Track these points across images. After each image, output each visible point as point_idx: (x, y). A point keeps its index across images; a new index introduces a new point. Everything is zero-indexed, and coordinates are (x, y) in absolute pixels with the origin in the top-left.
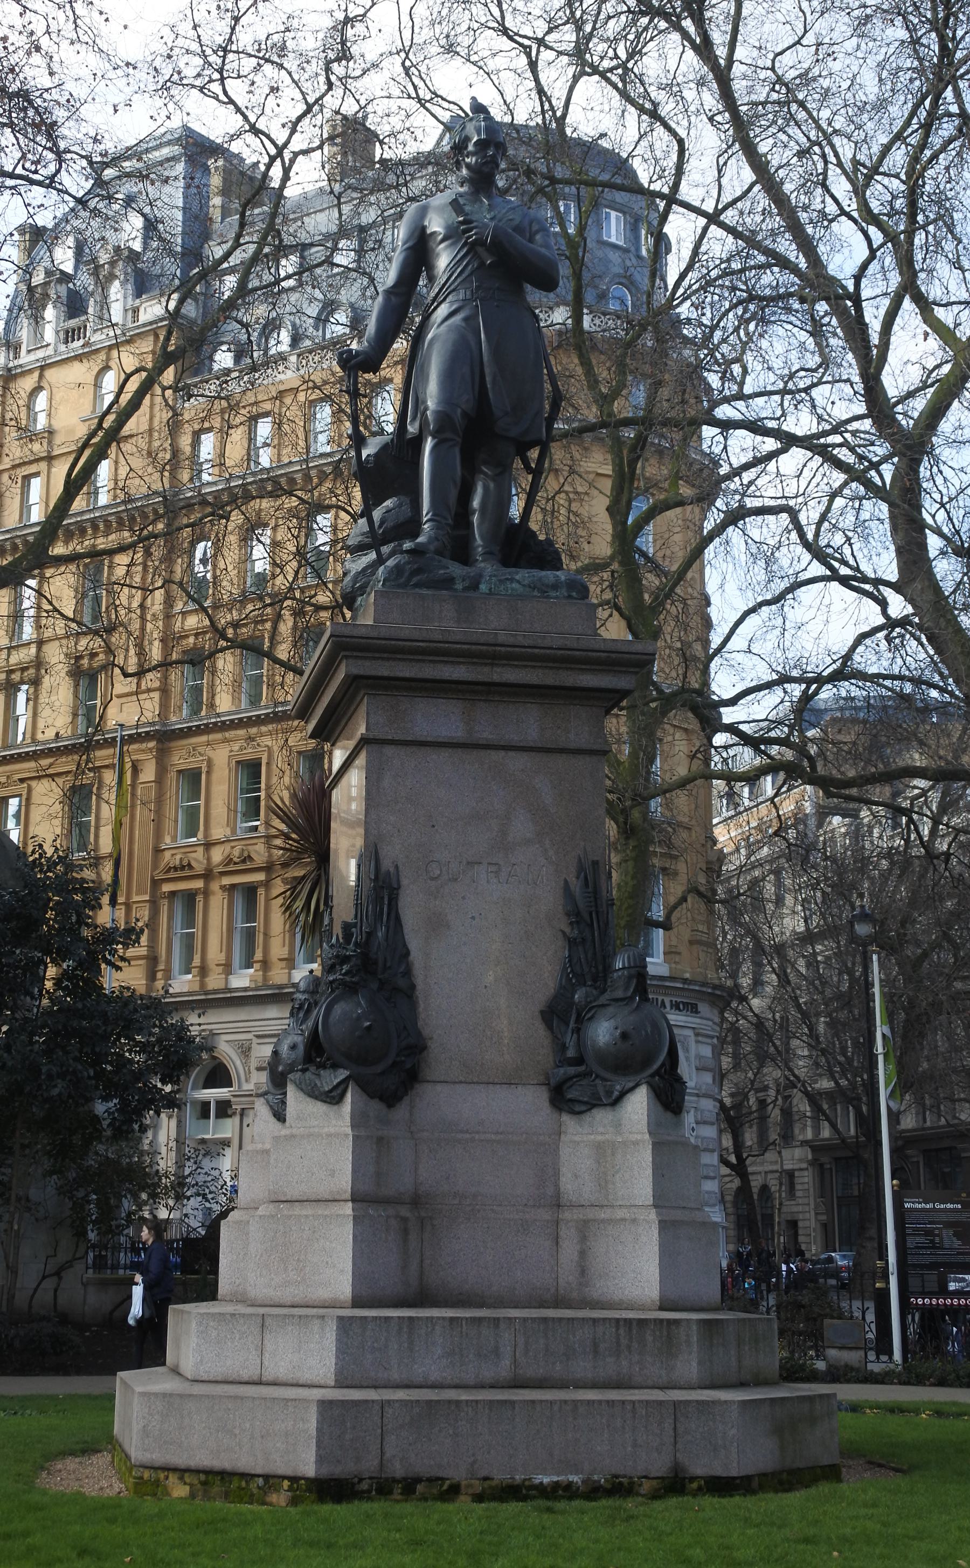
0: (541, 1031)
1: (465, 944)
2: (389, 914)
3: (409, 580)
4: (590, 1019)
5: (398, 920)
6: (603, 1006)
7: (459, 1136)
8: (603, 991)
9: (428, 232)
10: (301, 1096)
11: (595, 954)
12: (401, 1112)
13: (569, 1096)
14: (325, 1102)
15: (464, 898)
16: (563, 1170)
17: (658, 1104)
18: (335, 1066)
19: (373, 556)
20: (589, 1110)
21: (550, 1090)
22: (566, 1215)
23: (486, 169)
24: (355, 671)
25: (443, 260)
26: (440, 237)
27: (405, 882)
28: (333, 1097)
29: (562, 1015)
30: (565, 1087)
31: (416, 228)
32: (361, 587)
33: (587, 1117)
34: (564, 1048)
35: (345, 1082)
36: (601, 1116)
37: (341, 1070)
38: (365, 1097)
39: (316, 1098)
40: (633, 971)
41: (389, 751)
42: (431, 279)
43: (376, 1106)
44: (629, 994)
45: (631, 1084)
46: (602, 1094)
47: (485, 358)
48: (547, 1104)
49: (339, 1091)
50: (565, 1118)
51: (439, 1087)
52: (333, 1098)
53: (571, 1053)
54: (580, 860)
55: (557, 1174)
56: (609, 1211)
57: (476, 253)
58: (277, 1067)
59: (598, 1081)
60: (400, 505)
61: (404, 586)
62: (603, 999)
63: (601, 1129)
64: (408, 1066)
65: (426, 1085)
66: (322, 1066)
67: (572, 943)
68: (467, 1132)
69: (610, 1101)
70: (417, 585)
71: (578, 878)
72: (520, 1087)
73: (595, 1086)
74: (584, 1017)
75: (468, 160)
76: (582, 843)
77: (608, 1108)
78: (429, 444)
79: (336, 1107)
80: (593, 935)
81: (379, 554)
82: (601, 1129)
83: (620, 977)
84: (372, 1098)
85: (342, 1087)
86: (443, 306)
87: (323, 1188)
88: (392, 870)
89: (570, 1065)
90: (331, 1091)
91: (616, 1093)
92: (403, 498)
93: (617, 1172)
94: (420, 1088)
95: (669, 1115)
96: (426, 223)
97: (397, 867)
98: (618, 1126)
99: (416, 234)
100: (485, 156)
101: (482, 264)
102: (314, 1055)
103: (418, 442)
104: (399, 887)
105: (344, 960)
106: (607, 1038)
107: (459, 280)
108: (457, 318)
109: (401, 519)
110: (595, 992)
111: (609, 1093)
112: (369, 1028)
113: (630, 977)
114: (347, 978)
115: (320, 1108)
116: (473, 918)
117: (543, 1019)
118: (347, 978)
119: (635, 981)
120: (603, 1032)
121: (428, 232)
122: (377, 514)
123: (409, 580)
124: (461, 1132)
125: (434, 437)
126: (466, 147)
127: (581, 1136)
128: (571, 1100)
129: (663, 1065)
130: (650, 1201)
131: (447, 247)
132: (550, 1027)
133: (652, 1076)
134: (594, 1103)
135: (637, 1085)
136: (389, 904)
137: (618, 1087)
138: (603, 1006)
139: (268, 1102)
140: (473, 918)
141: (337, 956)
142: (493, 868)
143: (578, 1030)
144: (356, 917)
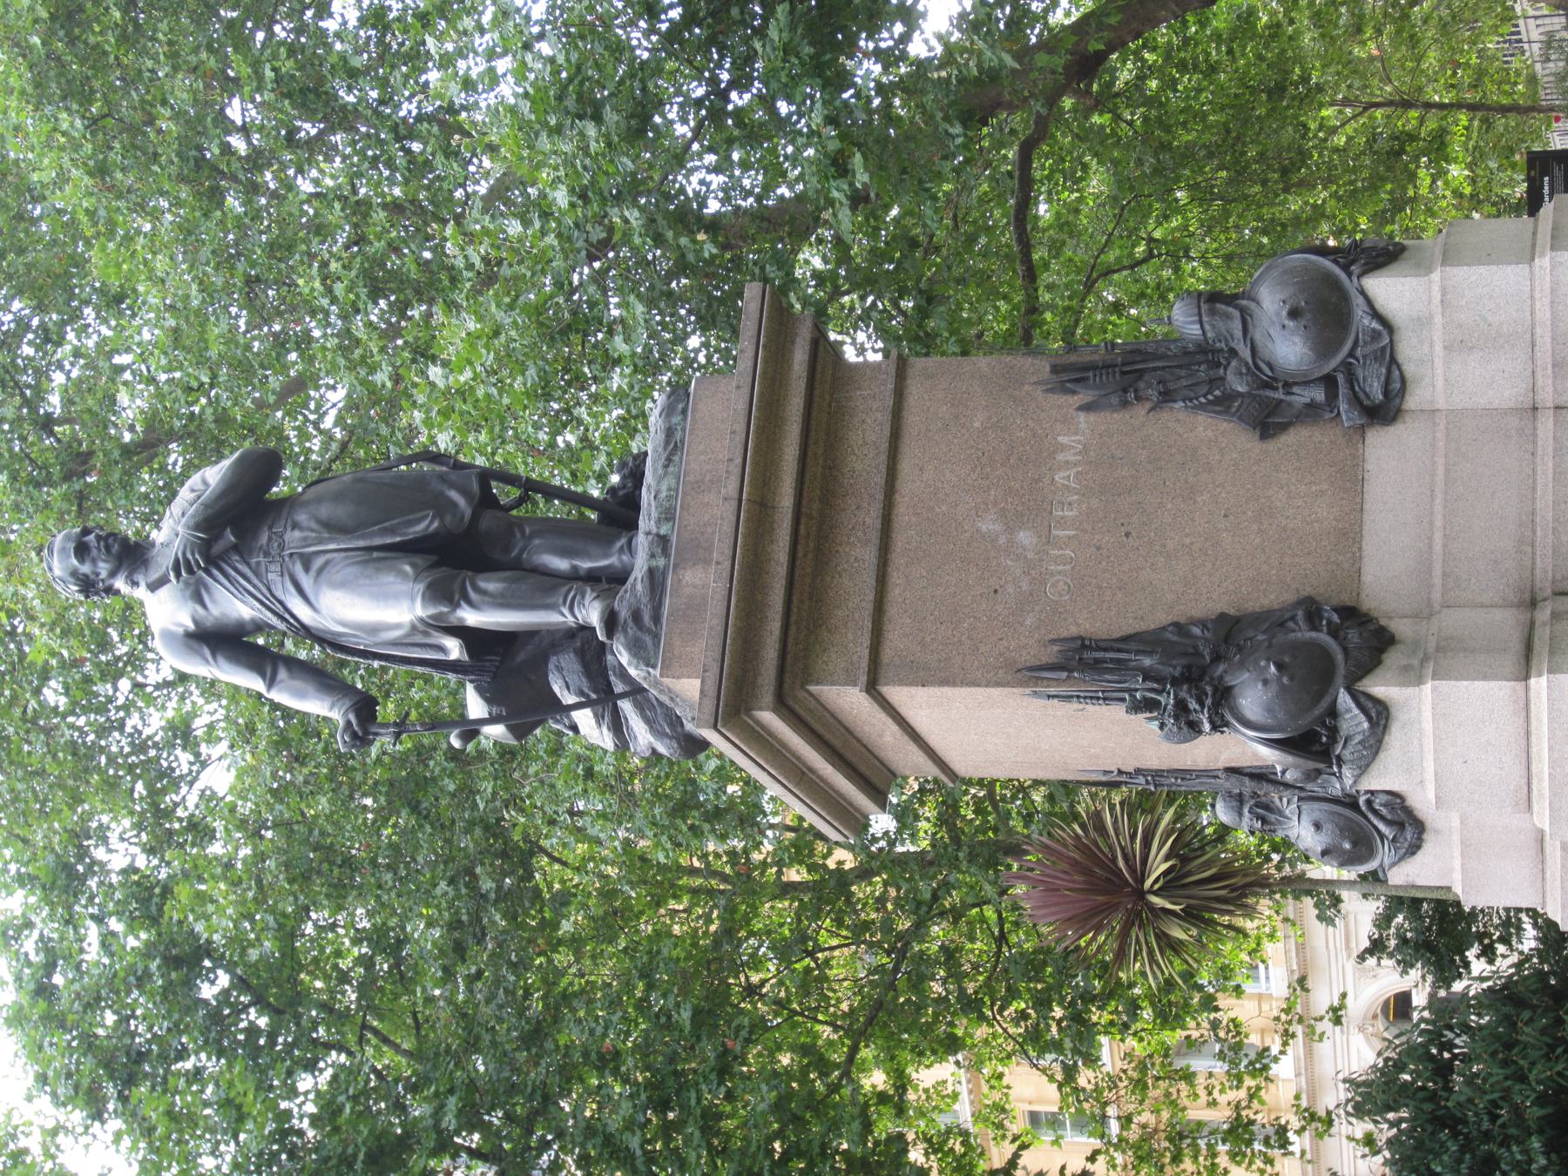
0: (1290, 439)
1: (1164, 546)
2: (1119, 650)
3: (649, 631)
4: (1271, 368)
5: (1126, 639)
7: (1438, 548)
8: (1233, 352)
9: (192, 627)
10: (1376, 768)
11: (1180, 367)
12: (1401, 627)
13: (1379, 397)
14: (1385, 727)
15: (1098, 548)
16: (1482, 402)
17: (1385, 271)
18: (1333, 712)
19: (626, 706)
21: (1372, 424)
22: (1546, 397)
23: (116, 548)
24: (767, 696)
26: (199, 609)
27: (1074, 631)
28: (1379, 715)
29: (1267, 410)
31: (191, 648)
32: (671, 725)
33: (1409, 369)
34: (1312, 406)
35: (1355, 696)
36: (1409, 351)
37: (1340, 700)
38: (1378, 671)
39: (1380, 742)
40: (1204, 307)
41: (887, 654)
42: (260, 627)
43: (1393, 658)
44: (1236, 313)
45: (1360, 300)
46: (1376, 346)
47: (361, 543)
48: (1391, 429)
49: (1370, 705)
50: (1412, 402)
52: (1379, 713)
53: (1319, 395)
54: (1047, 391)
55: (1488, 412)
56: (1538, 331)
58: (1345, 852)
59: (1359, 352)
60: (559, 669)
61: (656, 637)
62: (1246, 353)
63: (1426, 348)
64: (1335, 618)
66: (1334, 732)
67: (1167, 397)
69: (1385, 333)
70: (657, 618)
71: (1074, 392)
73: (1364, 357)
74: (1267, 378)
75: (104, 574)
76: (1026, 387)
77: (1395, 337)
78: (471, 617)
79: (1393, 711)
80: (1155, 369)
81: (623, 696)
82: (1426, 348)
83: (1213, 327)
85: (1362, 699)
86: (290, 605)
87: (1522, 693)
88: (1056, 648)
89: (1337, 396)
90: (1369, 718)
91: (1375, 325)
92: (551, 666)
93: (1485, 319)
94: (1368, 604)
95: (1406, 254)
96: (181, 630)
97: (1053, 641)
98: (1423, 322)
99: (195, 645)
101: (235, 548)
102: (1316, 748)
103: (471, 637)
104: (1083, 639)
105: (1181, 706)
106: (1297, 339)
107: (256, 581)
108: (306, 581)
110: (1234, 363)
111: (1376, 335)
112: (1279, 667)
113: (1213, 313)
114: (1209, 701)
115: (1395, 738)
117: (1273, 436)
118: (1209, 701)
119: (1218, 306)
120: (1289, 349)
121: (192, 627)
122: (569, 699)
123: (649, 631)
124: (1430, 546)
125: (458, 606)
126: (86, 576)
127: (1439, 375)
128: (1386, 393)
129: (1335, 262)
130: (1523, 269)
131: (214, 601)
132: (1284, 427)
133: (1349, 275)
134: (1390, 359)
135: (1363, 293)
136: (1105, 650)
137: (1366, 322)
139: (1393, 865)
140: (1127, 535)
141: (1176, 718)
143: (1288, 386)
144: (1123, 700)
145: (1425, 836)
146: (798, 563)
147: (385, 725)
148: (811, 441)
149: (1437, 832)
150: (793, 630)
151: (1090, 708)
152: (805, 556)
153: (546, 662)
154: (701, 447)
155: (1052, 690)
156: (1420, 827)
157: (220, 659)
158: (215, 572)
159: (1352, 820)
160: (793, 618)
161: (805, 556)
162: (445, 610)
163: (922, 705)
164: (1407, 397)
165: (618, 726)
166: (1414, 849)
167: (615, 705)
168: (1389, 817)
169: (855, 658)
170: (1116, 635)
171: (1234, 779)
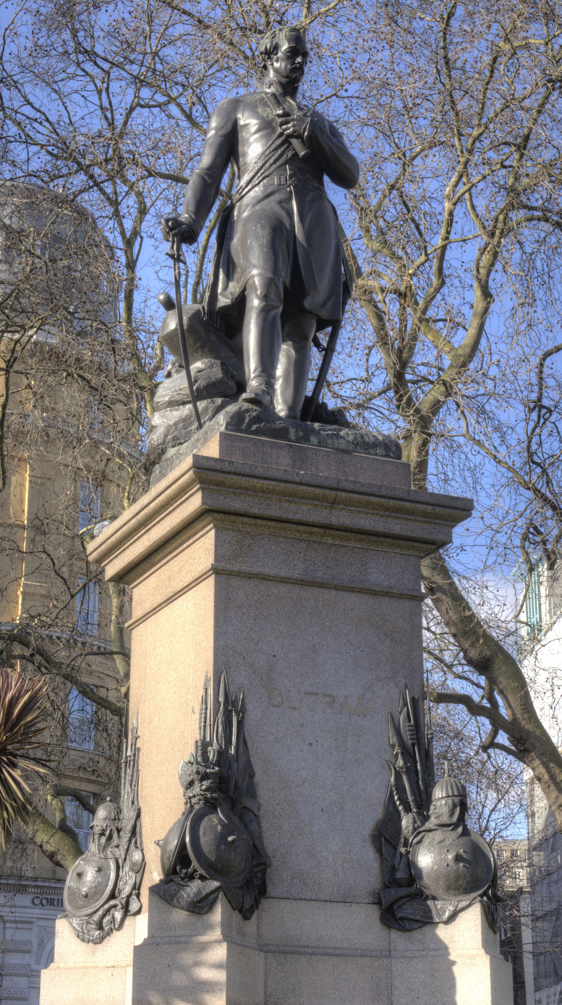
6: (430, 831)
13: (399, 915)
15: (302, 725)
20: (421, 927)
25: (254, 149)
30: (395, 907)
35: (218, 889)
43: (237, 916)
45: (464, 904)
48: (378, 922)
51: (282, 903)
57: (290, 144)
60: (211, 366)
65: (271, 901)
68: (308, 947)
72: (354, 906)
84: (234, 909)
86: (257, 189)
94: (265, 904)
100: (294, 63)
107: (274, 167)
109: (213, 379)
116: (310, 744)
117: (374, 842)
119: (458, 809)
128: (402, 919)
132: (379, 851)
138: (430, 831)
140: (310, 744)
142: (327, 699)
145: (91, 944)
146: (294, 526)
147: (179, 249)
148: (371, 538)
149: (94, 952)
150: (250, 521)
151: (197, 716)
152: (299, 531)
153: (216, 358)
154: (365, 466)
155: (211, 691)
156: (100, 940)
157: (222, 139)
158: (280, 140)
159: (102, 894)
160: (259, 522)
161: (299, 531)
162: (259, 292)
163: (200, 606)
164: (399, 933)
165: (173, 404)
166: (82, 937)
167: (189, 402)
168: (105, 921)
169: (233, 562)
170: (246, 734)
171: (133, 814)
